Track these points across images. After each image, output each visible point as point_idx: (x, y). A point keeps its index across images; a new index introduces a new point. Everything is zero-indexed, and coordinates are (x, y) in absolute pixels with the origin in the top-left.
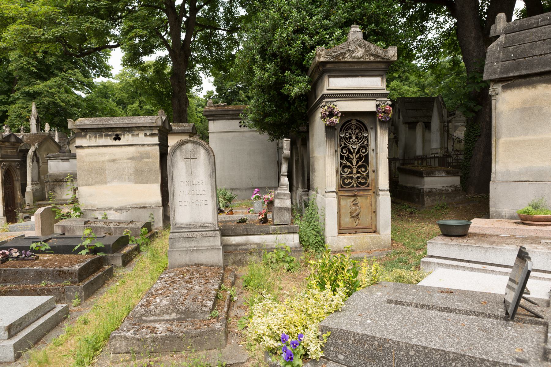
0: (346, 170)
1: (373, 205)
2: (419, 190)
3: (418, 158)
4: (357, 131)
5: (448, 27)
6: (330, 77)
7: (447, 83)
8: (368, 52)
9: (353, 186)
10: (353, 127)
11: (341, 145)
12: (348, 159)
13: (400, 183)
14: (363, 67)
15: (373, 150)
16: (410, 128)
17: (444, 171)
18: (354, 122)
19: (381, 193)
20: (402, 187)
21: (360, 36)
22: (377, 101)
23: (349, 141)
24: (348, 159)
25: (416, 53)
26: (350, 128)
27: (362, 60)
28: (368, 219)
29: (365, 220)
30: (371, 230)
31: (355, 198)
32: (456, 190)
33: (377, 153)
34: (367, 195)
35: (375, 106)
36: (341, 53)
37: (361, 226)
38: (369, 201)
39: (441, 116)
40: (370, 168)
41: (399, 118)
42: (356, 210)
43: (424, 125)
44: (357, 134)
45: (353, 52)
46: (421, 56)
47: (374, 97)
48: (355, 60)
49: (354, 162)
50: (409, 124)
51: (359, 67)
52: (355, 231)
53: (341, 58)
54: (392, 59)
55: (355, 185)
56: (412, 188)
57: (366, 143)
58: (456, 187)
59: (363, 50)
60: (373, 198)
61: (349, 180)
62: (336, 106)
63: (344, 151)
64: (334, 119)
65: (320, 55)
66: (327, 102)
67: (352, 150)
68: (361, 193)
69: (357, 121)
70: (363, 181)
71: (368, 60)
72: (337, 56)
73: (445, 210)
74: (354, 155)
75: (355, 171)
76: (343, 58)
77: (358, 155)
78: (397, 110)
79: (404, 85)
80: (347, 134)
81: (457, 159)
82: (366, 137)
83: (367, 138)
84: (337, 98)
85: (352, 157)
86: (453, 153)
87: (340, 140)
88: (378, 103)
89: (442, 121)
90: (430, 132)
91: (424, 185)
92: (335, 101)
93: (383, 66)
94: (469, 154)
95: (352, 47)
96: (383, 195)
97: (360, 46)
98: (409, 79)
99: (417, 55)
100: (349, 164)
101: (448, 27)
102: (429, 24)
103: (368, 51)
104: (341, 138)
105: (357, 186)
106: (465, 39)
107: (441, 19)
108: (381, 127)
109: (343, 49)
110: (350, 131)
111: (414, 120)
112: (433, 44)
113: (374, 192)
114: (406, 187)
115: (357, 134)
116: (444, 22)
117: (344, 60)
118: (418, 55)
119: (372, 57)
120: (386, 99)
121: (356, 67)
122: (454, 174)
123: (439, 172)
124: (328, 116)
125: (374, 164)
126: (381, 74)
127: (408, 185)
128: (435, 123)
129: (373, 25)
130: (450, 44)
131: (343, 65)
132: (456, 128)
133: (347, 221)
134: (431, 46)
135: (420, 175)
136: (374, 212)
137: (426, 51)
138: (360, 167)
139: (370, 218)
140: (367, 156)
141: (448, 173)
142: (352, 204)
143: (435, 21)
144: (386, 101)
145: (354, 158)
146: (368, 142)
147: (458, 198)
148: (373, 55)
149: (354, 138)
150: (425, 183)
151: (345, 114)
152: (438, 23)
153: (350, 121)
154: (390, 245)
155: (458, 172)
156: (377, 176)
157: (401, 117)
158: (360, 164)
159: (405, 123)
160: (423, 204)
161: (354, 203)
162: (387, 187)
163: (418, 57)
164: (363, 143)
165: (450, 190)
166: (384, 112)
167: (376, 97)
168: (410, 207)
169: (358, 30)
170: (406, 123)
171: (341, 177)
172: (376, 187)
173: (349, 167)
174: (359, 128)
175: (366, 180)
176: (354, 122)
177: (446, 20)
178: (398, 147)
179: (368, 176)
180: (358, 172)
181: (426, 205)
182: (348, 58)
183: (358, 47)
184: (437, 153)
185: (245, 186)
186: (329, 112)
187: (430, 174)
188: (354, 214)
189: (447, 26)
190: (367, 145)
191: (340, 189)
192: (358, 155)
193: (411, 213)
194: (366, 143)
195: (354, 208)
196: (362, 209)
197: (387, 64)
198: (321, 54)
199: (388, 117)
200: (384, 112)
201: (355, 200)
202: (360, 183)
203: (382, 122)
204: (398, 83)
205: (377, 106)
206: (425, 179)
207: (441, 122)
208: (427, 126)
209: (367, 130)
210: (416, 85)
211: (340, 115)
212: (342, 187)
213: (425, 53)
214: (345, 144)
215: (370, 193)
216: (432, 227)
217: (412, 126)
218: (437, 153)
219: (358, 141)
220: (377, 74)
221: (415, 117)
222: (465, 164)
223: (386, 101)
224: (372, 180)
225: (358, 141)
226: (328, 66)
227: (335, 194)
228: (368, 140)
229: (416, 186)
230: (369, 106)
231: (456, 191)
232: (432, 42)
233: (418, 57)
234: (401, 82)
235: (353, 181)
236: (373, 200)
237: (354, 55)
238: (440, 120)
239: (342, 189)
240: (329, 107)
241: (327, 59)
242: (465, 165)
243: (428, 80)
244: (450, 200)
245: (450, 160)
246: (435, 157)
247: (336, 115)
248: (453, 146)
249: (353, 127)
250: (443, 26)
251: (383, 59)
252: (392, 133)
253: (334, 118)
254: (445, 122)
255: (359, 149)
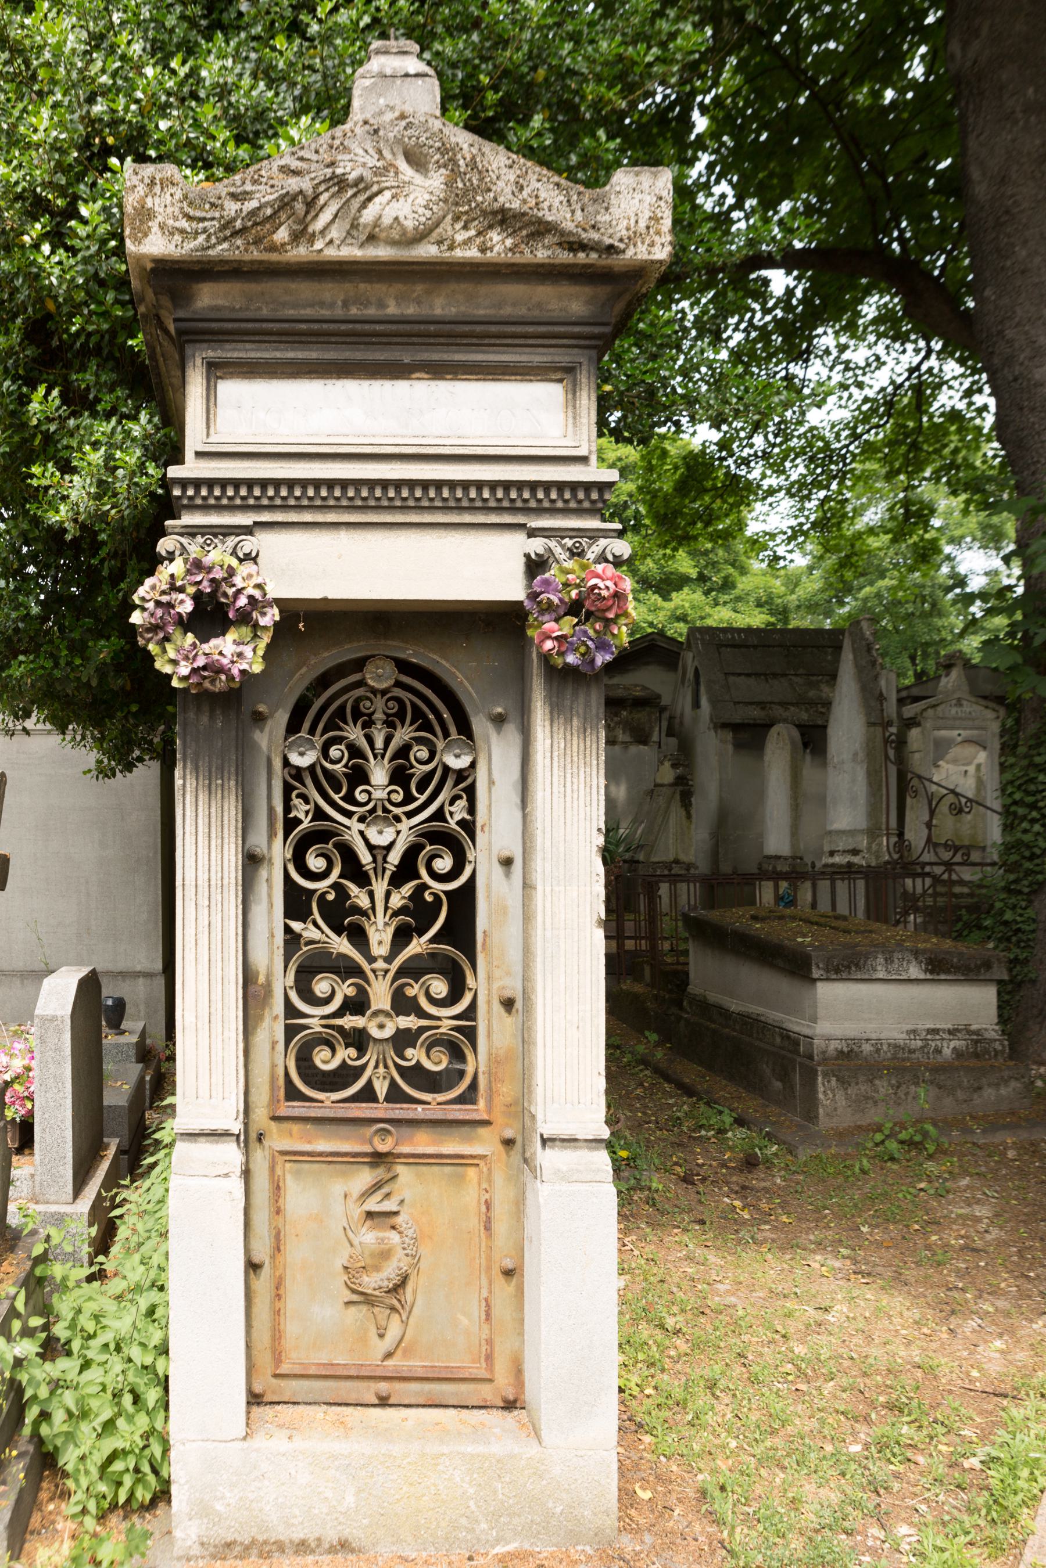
0: (321, 986)
1: (502, 1226)
2: (791, 1041)
3: (770, 870)
4: (403, 734)
5: (885, 382)
6: (216, 370)
7: (865, 600)
8: (465, 201)
9: (368, 1094)
10: (379, 708)
11: (291, 824)
12: (341, 916)
13: (695, 988)
14: (442, 305)
15: (507, 863)
16: (738, 746)
17: (916, 953)
18: (380, 676)
19: (547, 1159)
20: (705, 1007)
21: (423, 97)
22: (532, 533)
23: (350, 799)
24: (341, 916)
25: (764, 476)
26: (357, 714)
27: (428, 251)
28: (470, 1319)
29: (444, 1320)
30: (486, 1393)
31: (380, 1173)
32: (976, 1051)
33: (527, 886)
34: (459, 1160)
35: (519, 566)
36: (286, 202)
37: (416, 1364)
38: (471, 1196)
39: (871, 696)
40: (485, 982)
41: (696, 705)
42: (385, 1255)
43: (796, 733)
44: (404, 752)
45: (363, 190)
46: (780, 489)
47: (513, 510)
48: (382, 252)
49: (380, 935)
50: (736, 728)
51: (411, 310)
52: (381, 1388)
53: (282, 235)
54: (638, 253)
55: (381, 1088)
56: (751, 1024)
57: (458, 811)
58: (977, 1038)
59: (436, 181)
60: (499, 1179)
61: (345, 1054)
62: (251, 558)
63: (315, 863)
64: (225, 646)
65: (145, 214)
66: (191, 532)
67: (365, 857)
68: (423, 1143)
69: (403, 666)
70: (437, 1063)
71: (472, 253)
72: (255, 227)
73: (930, 1166)
74: (380, 887)
75: (380, 995)
76: (296, 237)
77: (407, 889)
78: (690, 674)
79: (717, 604)
80: (334, 752)
81: (952, 883)
82: (461, 775)
83: (465, 783)
84: (258, 508)
85: (364, 902)
86: (927, 857)
87: (288, 789)
88: (537, 546)
89: (876, 721)
90: (824, 764)
91: (814, 1019)
92: (247, 531)
93: (573, 303)
94: (1029, 873)
95: (358, 160)
96: (565, 1178)
97: (416, 159)
98: (733, 586)
99: (766, 484)
100: (341, 945)
101: (885, 382)
102: (811, 374)
103: (470, 191)
104: (298, 773)
105: (395, 1095)
106: (1009, 334)
107: (859, 355)
108: (557, 709)
109: (296, 173)
110: (355, 734)
111: (755, 714)
112: (827, 444)
113: (509, 1143)
114: (725, 1014)
115: (404, 752)
116: (868, 365)
117: (301, 253)
118: (772, 481)
119: (495, 236)
120: (595, 524)
121: (392, 309)
122: (968, 972)
123: (889, 960)
124: (186, 624)
125: (514, 955)
126: (563, 357)
127: (734, 1006)
128: (848, 728)
129: (537, 121)
130: (891, 443)
131: (305, 289)
132: (941, 748)
133: (321, 1321)
134: (820, 450)
135: (798, 967)
136: (508, 1273)
137: (801, 469)
138: (413, 970)
139: (477, 1311)
140: (464, 901)
141: (939, 967)
142: (358, 1212)
143: (836, 362)
144: (594, 535)
145: (381, 904)
146: (472, 809)
147: (989, 1093)
148: (503, 218)
149: (379, 775)
150: (821, 1012)
151: (307, 623)
152: (847, 369)
153: (359, 664)
154: (611, 1522)
155: (987, 965)
156: (526, 1038)
157: (704, 701)
158: (417, 946)
159: (721, 725)
160: (811, 1116)
161: (373, 1204)
162: (594, 1122)
163: (771, 492)
164: (439, 815)
165: (947, 1052)
166: (574, 608)
167: (526, 510)
168: (740, 1122)
169: (413, 65)
170: (724, 726)
171: (291, 1032)
172: (521, 1109)
173: (347, 969)
174: (418, 714)
175: (457, 1053)
176: (380, 676)
177: (878, 358)
178: (689, 816)
179: (470, 1034)
180: (402, 1004)
181: (824, 1122)
182: (333, 244)
183: (402, 165)
184: (855, 852)
185: (20, 965)
186: (197, 597)
187: (848, 966)
188: (370, 1282)
189: (880, 379)
190: (469, 827)
191: (283, 1112)
192: (407, 889)
193: (750, 1163)
194: (458, 811)
195: (369, 1237)
196: (424, 1251)
197: (603, 291)
198: (161, 213)
199: (602, 646)
200: (574, 608)
201: (377, 1187)
202: (417, 1076)
203: (564, 679)
204: (698, 596)
205: (535, 566)
206: (820, 985)
207: (870, 724)
208: (813, 740)
209: (465, 729)
210: (759, 605)
211: (270, 617)
212: (292, 1094)
213: (794, 477)
214: (319, 814)
215: (483, 1144)
216: (879, 1312)
217: (749, 736)
218: (855, 852)
219: (409, 799)
220: (537, 357)
221: (762, 705)
222: (1008, 916)
223: (594, 535)
224: (494, 1060)
225: (409, 799)
226: (208, 297)
227: (231, 1154)
228: (471, 792)
229: (773, 1015)
230: (480, 567)
231: (976, 1055)
232: (822, 438)
233: (771, 492)
234: (706, 593)
235: (371, 1056)
236: (502, 1195)
237: (368, 215)
238: (868, 714)
239: (297, 1108)
240: (197, 565)
241: (190, 245)
242: (1006, 923)
243: (800, 592)
244: (948, 1101)
245: (912, 885)
246: (849, 871)
247: (244, 618)
248: (929, 825)
249: (379, 708)
250: (866, 379)
251: (577, 246)
252: (667, 764)
253: (231, 636)
254: (890, 723)
255: (411, 854)
